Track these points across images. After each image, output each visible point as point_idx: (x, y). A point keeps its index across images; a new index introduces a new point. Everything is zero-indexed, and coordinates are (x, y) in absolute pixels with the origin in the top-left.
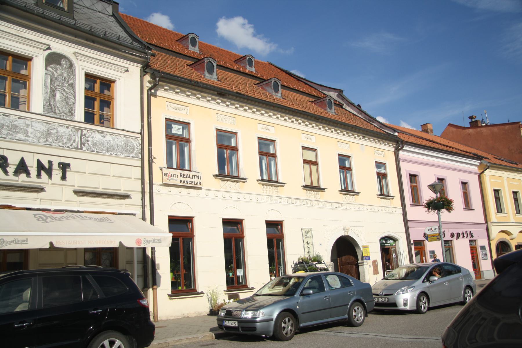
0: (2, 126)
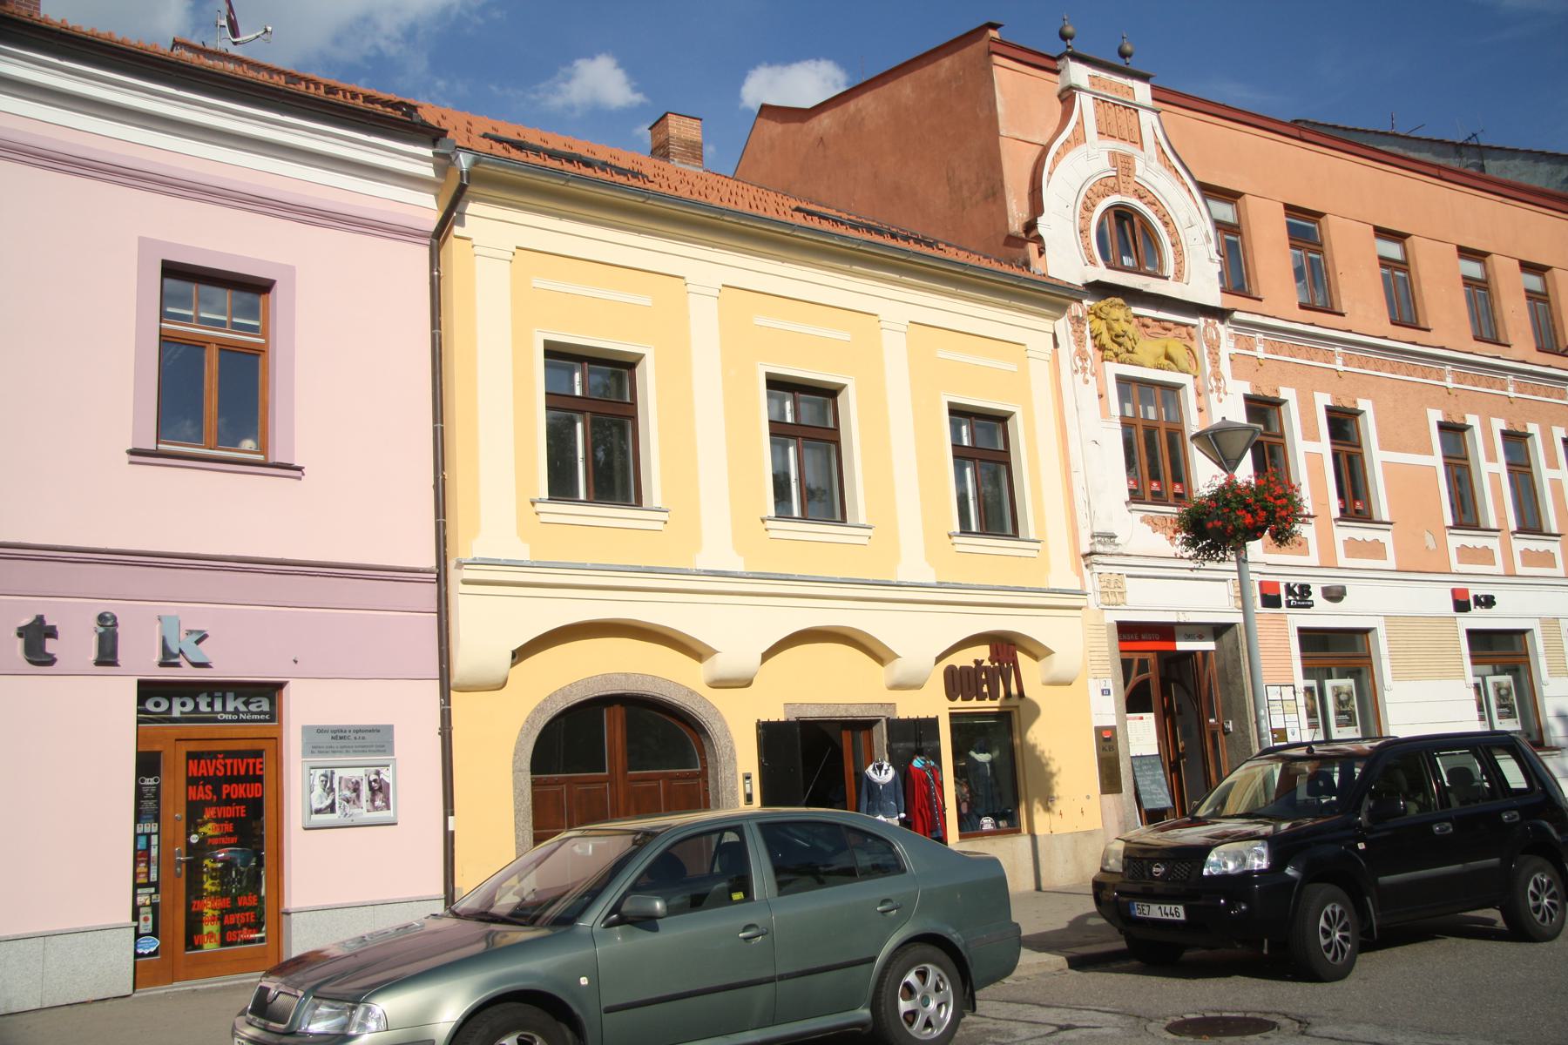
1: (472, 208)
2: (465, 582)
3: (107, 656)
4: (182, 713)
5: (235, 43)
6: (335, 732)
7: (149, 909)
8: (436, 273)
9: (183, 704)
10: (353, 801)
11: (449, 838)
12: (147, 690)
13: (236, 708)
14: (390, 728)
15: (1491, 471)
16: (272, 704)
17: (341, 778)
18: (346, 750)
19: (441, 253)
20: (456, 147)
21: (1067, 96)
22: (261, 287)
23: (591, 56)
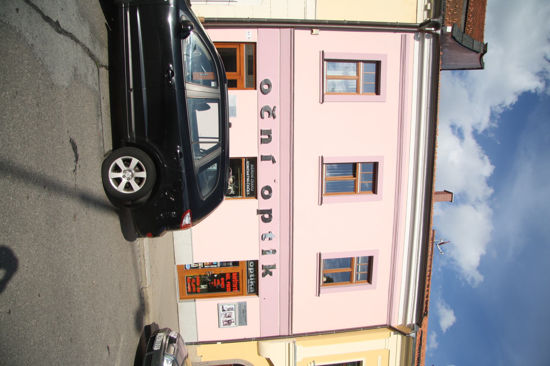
1: (400, 336)
2: (289, 344)
3: (264, 252)
4: (250, 270)
5: (437, 245)
6: (245, 310)
7: (197, 266)
8: (379, 327)
9: (252, 271)
10: (226, 316)
11: (214, 342)
12: (256, 263)
13: (251, 284)
14: (246, 325)
16: (252, 293)
17: (232, 312)
18: (240, 313)
19: (386, 328)
20: (417, 332)
22: (374, 190)
23: (455, 314)
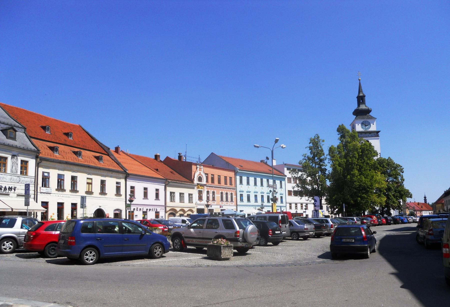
0: (1, 177)
15: (224, 196)
21: (197, 168)
